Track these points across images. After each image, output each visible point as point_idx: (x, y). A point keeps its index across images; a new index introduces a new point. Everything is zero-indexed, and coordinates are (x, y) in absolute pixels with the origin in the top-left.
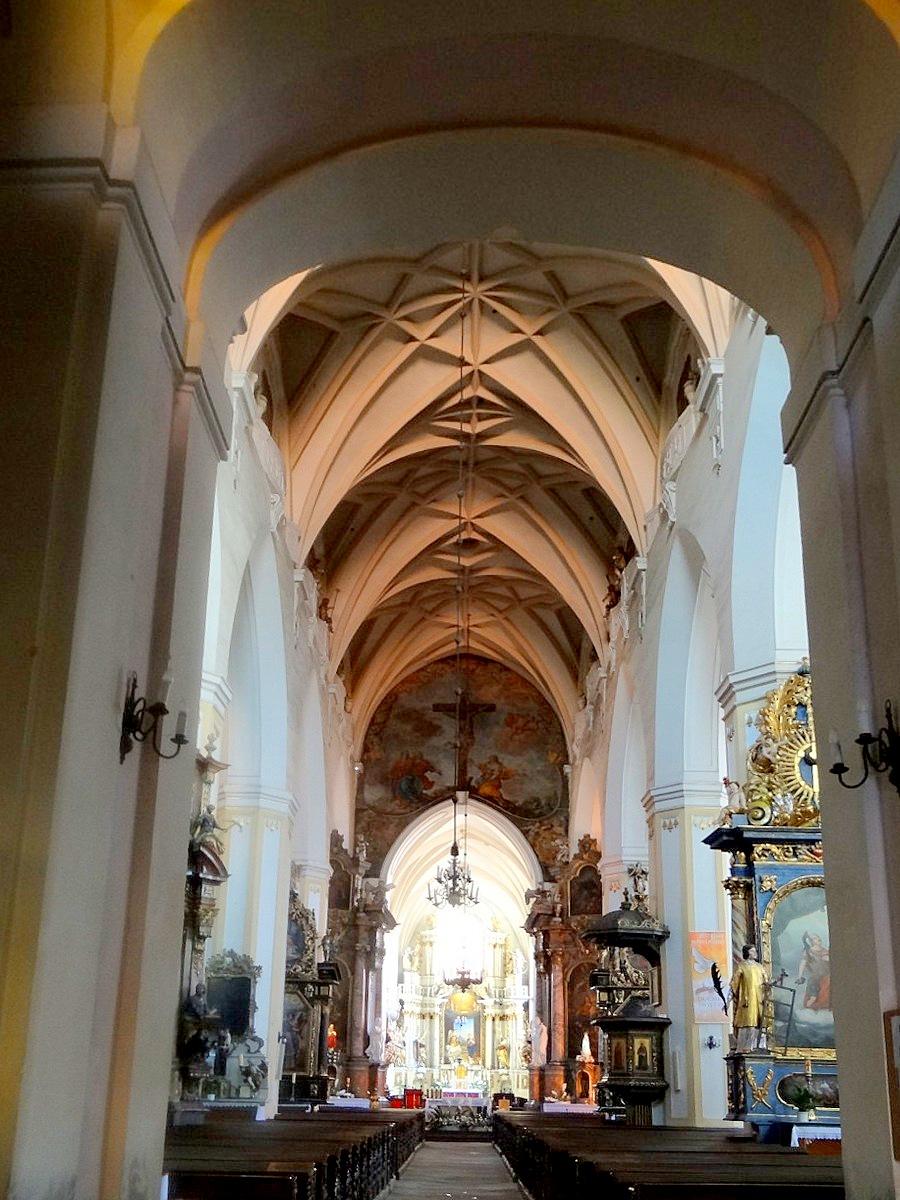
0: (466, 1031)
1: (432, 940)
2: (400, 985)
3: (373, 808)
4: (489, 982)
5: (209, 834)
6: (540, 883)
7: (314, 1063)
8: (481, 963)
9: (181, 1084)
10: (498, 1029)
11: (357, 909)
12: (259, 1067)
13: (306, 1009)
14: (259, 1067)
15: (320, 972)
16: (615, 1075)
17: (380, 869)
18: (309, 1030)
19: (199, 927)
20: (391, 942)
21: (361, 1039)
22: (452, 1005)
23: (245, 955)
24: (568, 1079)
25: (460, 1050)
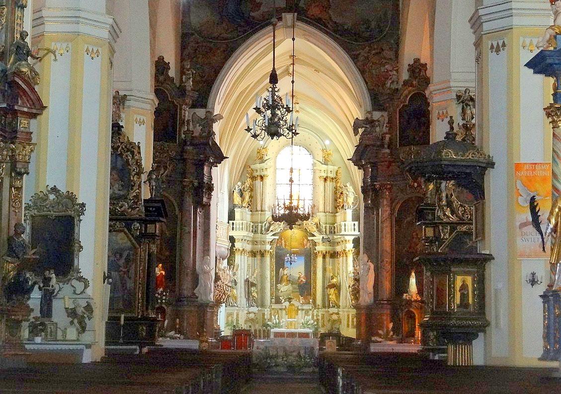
0: (296, 269)
1: (262, 174)
2: (231, 222)
3: (200, 33)
4: (321, 217)
6: (369, 112)
8: (306, 195)
10: (329, 267)
11: (185, 141)
15: (146, 208)
16: (437, 313)
17: (207, 99)
20: (221, 177)
21: (189, 278)
22: (283, 242)
24: (394, 317)
25: (291, 288)
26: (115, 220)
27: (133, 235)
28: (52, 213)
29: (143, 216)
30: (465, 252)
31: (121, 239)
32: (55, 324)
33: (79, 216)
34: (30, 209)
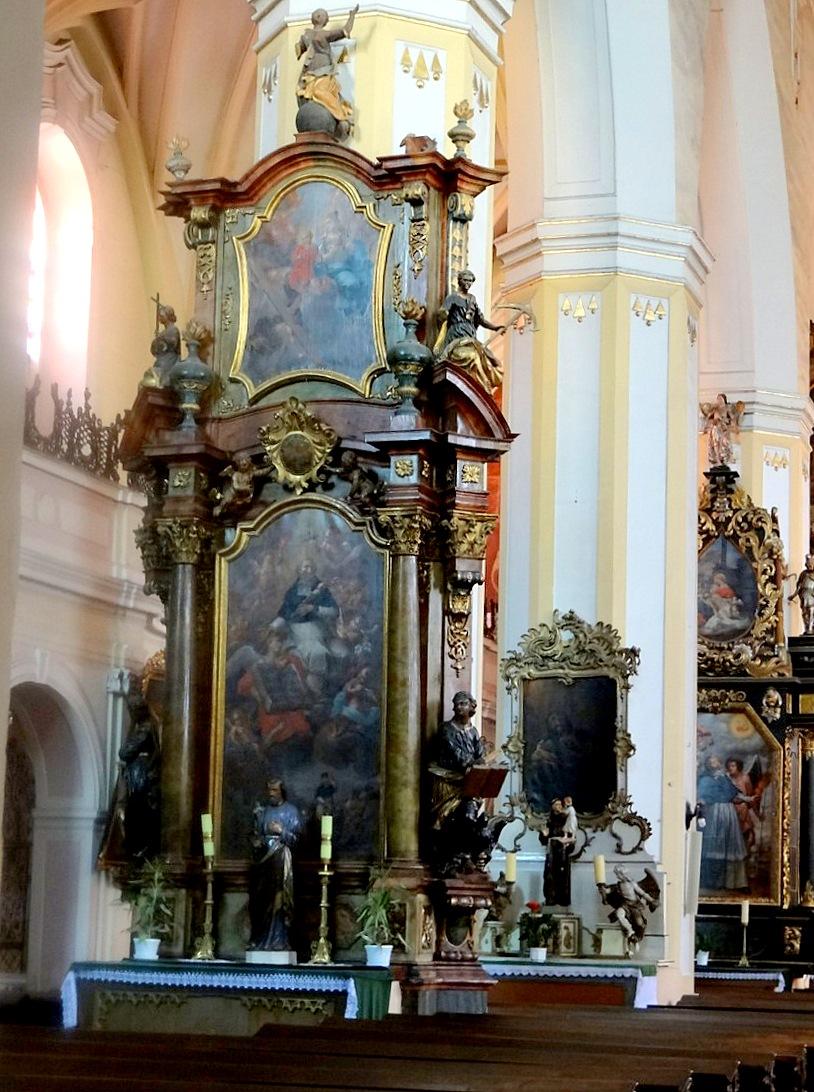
5: (466, 340)
7: (792, 873)
9: (431, 921)
12: (642, 884)
13: (768, 749)
14: (642, 884)
15: (795, 658)
18: (775, 798)
19: (453, 559)
23: (600, 624)
26: (718, 686)
27: (765, 720)
28: (567, 671)
29: (789, 675)
30: (550, 719)
31: (739, 729)
32: (576, 921)
33: (626, 677)
34: (519, 664)
